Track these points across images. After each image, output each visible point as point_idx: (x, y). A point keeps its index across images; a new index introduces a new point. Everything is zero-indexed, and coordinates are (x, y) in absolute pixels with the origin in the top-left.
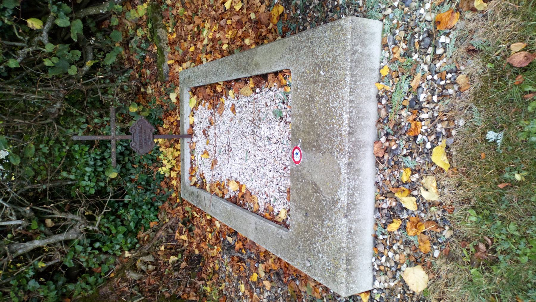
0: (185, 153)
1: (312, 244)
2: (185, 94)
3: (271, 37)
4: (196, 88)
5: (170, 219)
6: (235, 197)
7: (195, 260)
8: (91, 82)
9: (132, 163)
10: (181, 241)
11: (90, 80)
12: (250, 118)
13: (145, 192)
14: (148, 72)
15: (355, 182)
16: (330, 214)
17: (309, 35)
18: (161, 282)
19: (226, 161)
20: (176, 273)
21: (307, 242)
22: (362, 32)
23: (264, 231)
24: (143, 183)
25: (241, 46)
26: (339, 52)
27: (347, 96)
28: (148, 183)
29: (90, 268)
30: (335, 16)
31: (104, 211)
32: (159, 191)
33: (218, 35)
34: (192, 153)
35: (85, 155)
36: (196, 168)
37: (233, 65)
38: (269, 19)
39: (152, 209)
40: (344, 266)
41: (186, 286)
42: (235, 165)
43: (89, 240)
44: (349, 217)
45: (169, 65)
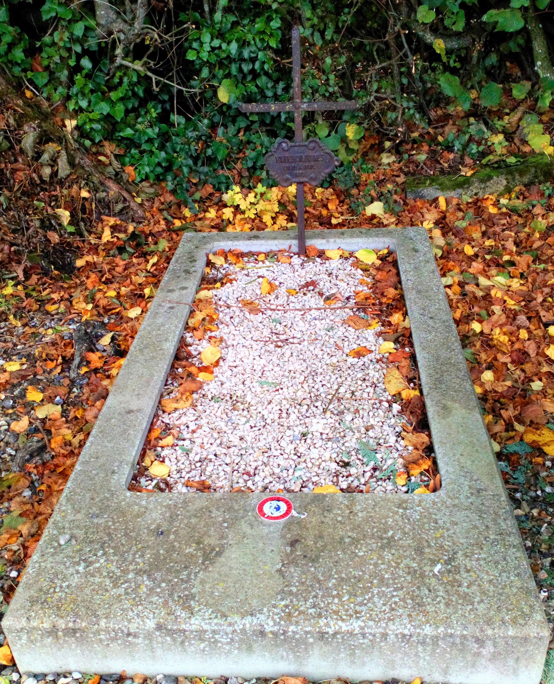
0: (271, 242)
1: (102, 547)
2: (382, 240)
3: (499, 428)
4: (395, 264)
5: (141, 205)
6: (190, 355)
7: (63, 259)
8: (403, 47)
9: (248, 129)
10: (100, 229)
11: (406, 46)
12: (342, 390)
13: (191, 157)
14: (422, 157)
15: (228, 643)
16: (163, 590)
17: (509, 535)
18: (19, 194)
19: (256, 335)
20: (37, 224)
21: (106, 537)
22: (520, 654)
23: (125, 431)
24: (209, 152)
25: (478, 363)
26: (481, 608)
27: (395, 628)
28: (210, 160)
29: (40, 50)
30: (543, 575)
31: (154, 77)
32: (194, 181)
33: (497, 309)
34: (270, 255)
35: (262, 40)
36: (240, 265)
37: (444, 354)
38: (532, 422)
39: (159, 170)
40: (61, 624)
41: (12, 245)
42: (251, 357)
43: (95, 48)
44: (158, 633)
45: (436, 199)
